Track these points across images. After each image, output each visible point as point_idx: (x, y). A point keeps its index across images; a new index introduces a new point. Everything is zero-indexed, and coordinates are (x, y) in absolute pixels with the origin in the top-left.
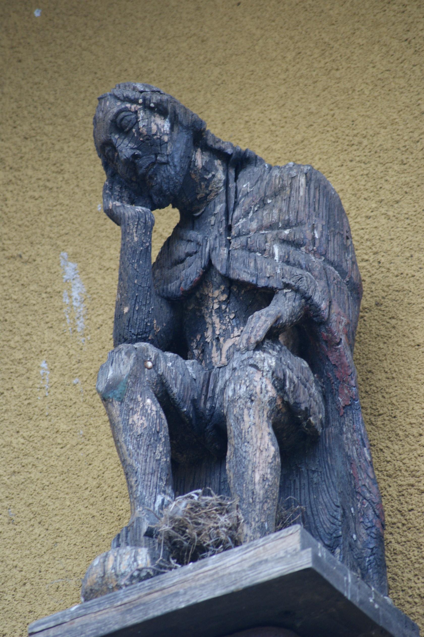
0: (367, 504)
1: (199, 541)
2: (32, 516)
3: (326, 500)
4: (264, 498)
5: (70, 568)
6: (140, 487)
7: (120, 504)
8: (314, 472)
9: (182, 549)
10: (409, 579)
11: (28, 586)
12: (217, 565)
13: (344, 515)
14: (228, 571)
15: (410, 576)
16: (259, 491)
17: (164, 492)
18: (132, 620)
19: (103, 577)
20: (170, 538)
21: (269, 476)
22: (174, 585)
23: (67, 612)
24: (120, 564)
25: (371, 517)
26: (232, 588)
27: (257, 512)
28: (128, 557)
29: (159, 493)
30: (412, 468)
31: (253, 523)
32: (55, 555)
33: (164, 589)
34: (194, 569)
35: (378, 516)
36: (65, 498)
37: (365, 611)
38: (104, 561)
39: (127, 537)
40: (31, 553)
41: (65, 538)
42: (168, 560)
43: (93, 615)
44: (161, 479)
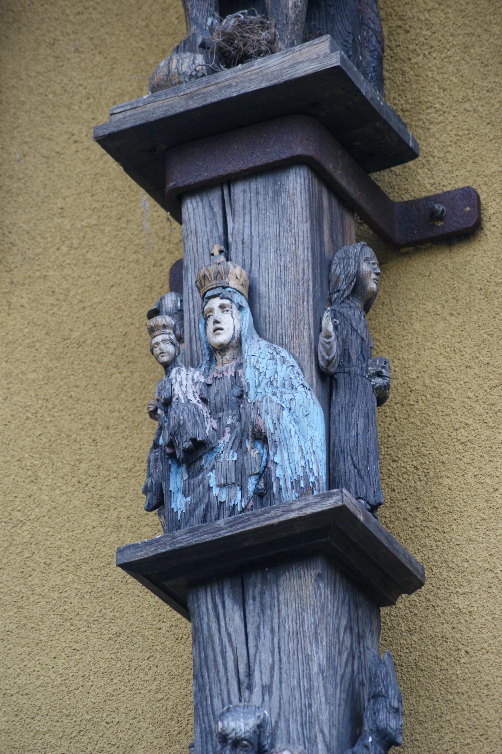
0: (371, 33)
1: (244, 51)
2: (93, 47)
3: (340, 28)
4: (295, 21)
5: (124, 88)
6: (194, 10)
7: (164, 40)
8: (331, 6)
9: (229, 55)
10: (394, 98)
11: (91, 100)
12: (261, 65)
13: (354, 40)
14: (271, 70)
15: (396, 95)
16: (292, 15)
17: (213, 16)
18: (193, 105)
19: (168, 75)
20: (220, 49)
21: (299, 4)
22: (226, 80)
23: (140, 99)
24: (182, 65)
25: (374, 43)
26: (275, 82)
27: (290, 31)
28: (188, 60)
29: (210, 16)
30: (400, 13)
31: (286, 40)
32: (112, 78)
33: (219, 83)
34: (243, 69)
35: (380, 43)
36: (120, 35)
37: (374, 106)
38: (169, 63)
39: (186, 46)
40: (93, 75)
41: (119, 65)
42: (219, 65)
43: (161, 102)
44: (211, 5)
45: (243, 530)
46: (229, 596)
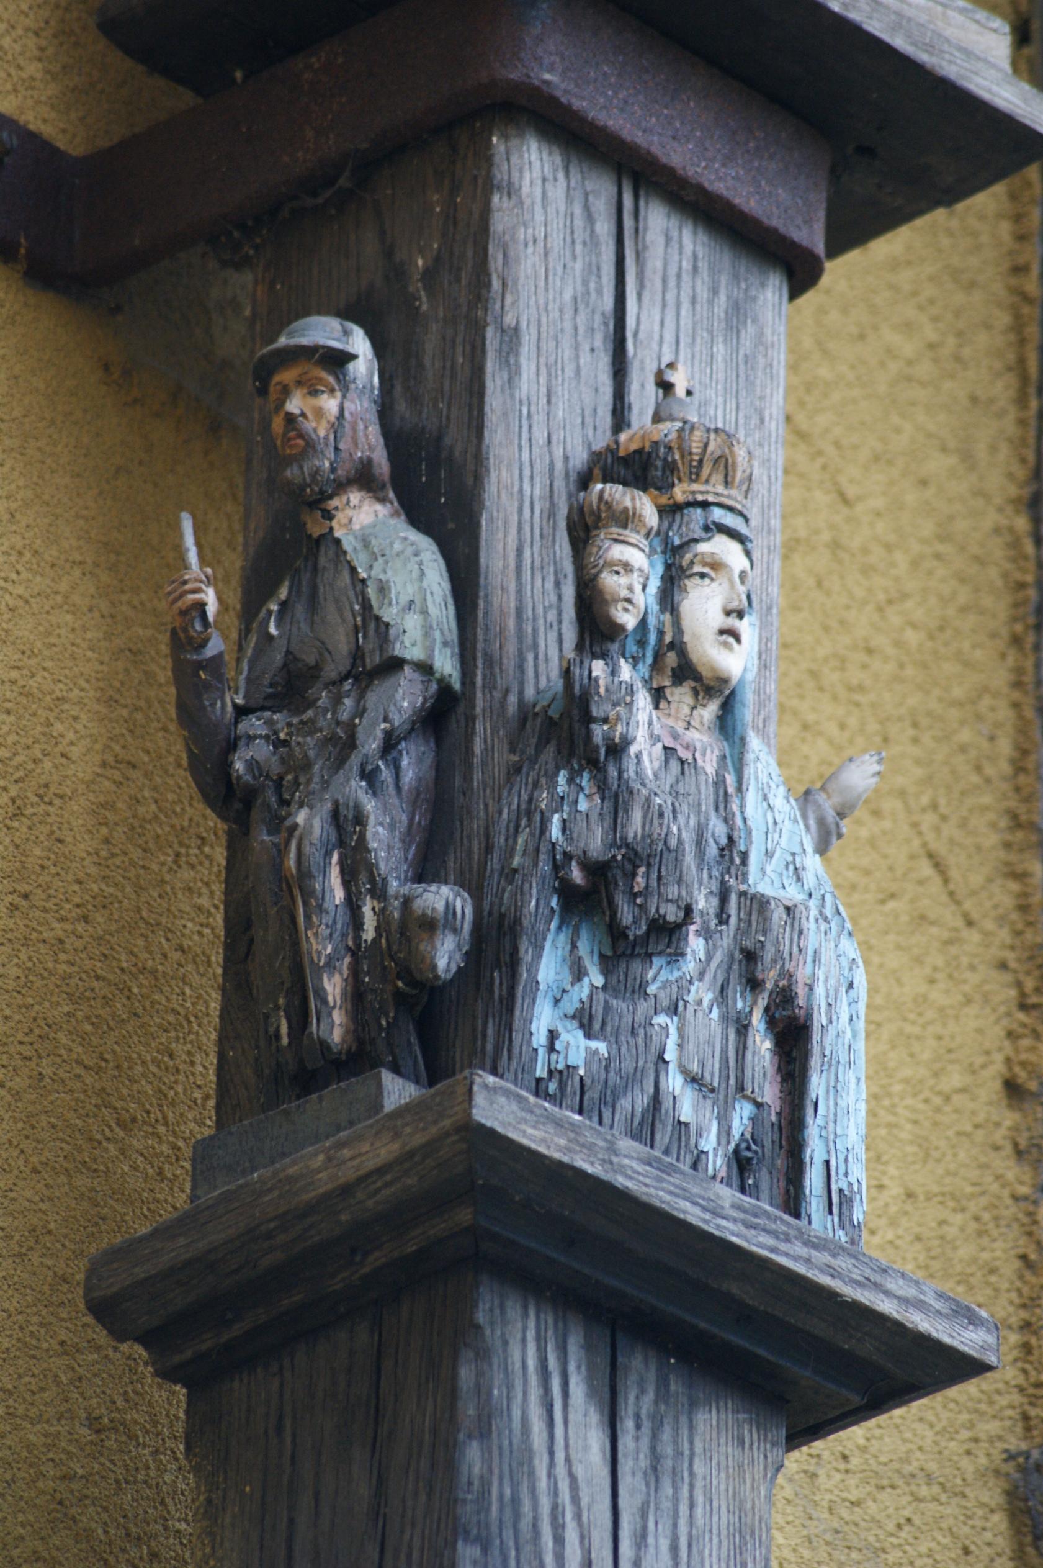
45: (773, 1256)
46: (579, 1367)
